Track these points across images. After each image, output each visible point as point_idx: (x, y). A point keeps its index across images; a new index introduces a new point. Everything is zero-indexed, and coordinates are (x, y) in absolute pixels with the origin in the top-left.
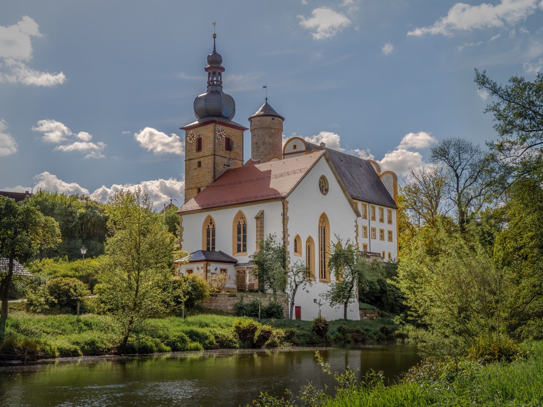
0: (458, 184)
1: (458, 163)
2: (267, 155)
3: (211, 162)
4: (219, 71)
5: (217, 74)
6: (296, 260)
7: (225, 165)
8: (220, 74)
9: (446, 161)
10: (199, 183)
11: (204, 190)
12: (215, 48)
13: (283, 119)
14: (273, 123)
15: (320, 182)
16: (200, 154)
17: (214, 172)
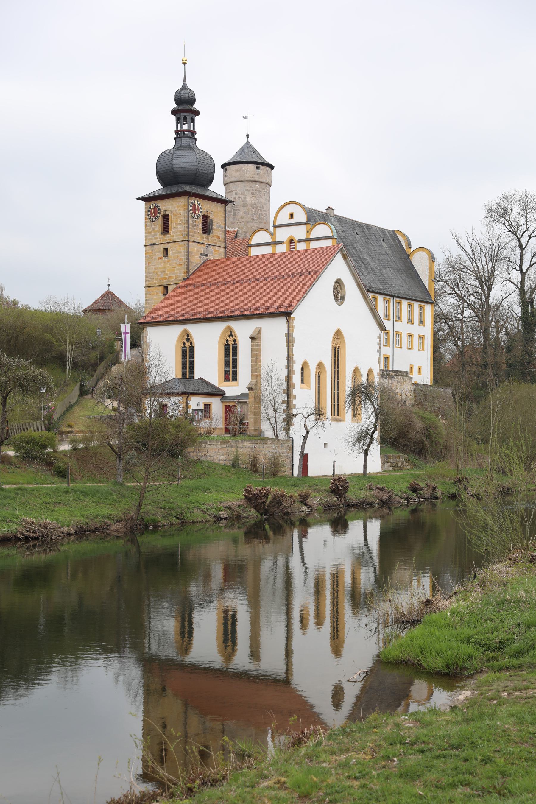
0: (521, 259)
1: (523, 228)
2: (248, 222)
3: (183, 250)
4: (193, 116)
5: (189, 120)
6: (304, 398)
7: (201, 254)
8: (193, 120)
9: (507, 223)
10: (165, 278)
11: (174, 291)
12: (185, 80)
13: (272, 167)
14: (258, 174)
15: (334, 287)
16: (167, 238)
17: (188, 265)
